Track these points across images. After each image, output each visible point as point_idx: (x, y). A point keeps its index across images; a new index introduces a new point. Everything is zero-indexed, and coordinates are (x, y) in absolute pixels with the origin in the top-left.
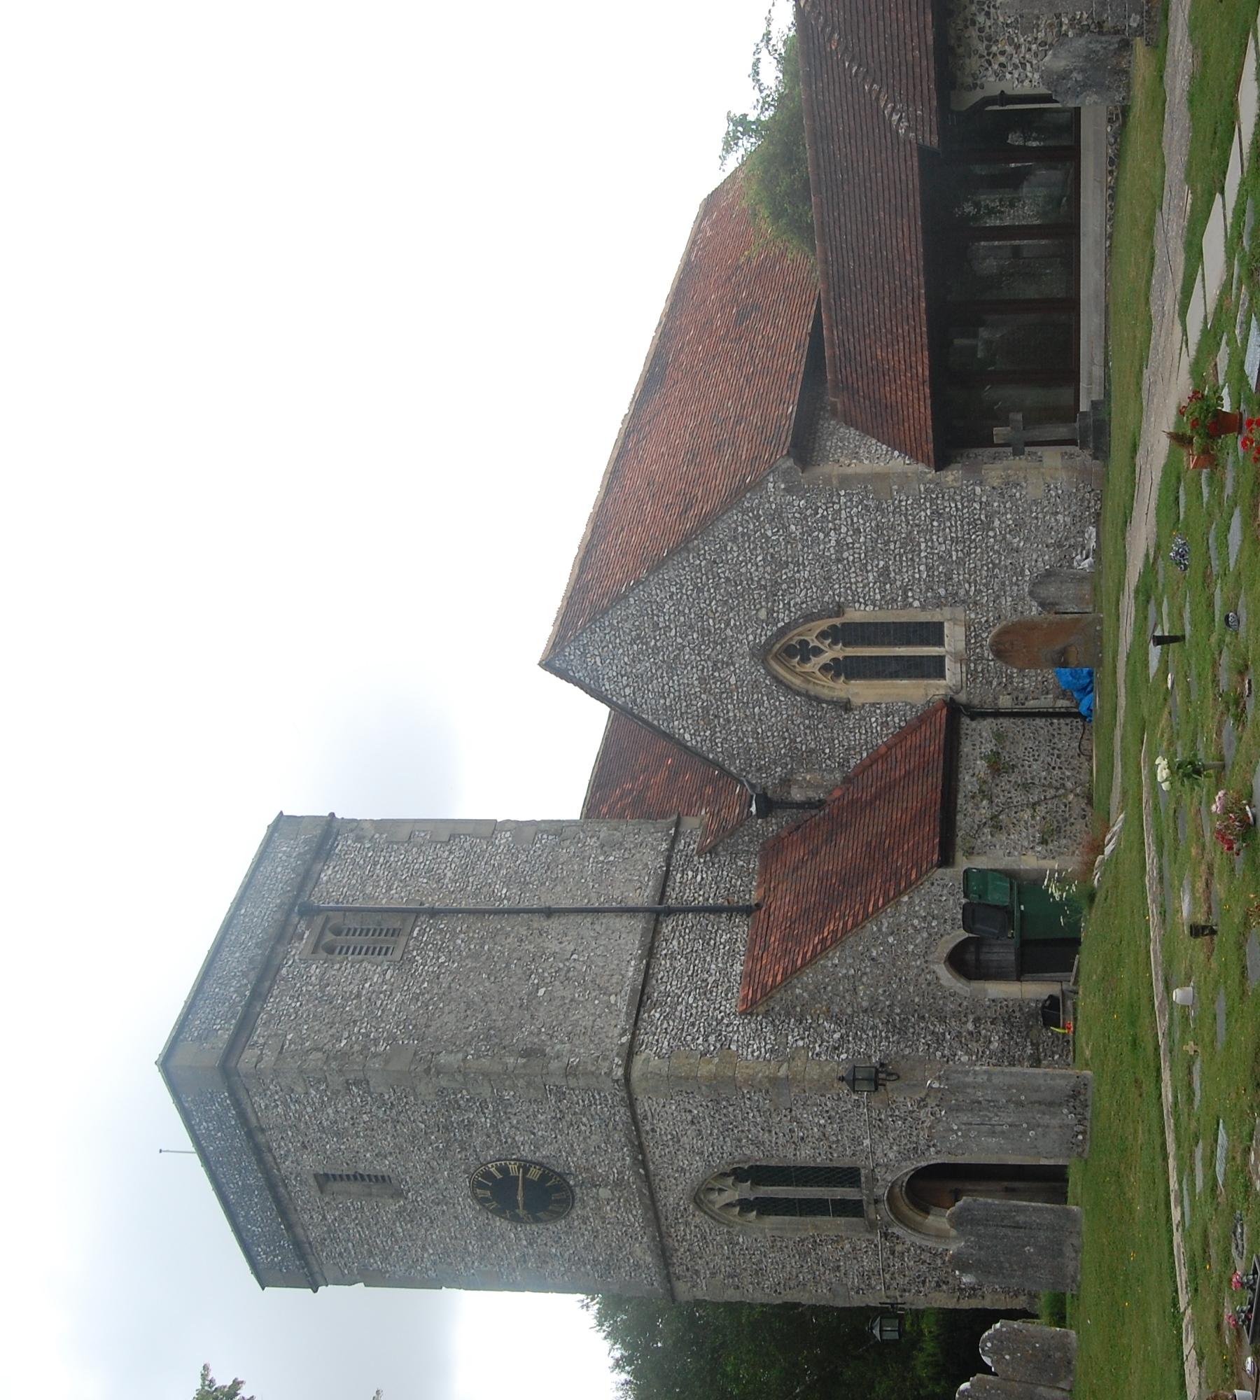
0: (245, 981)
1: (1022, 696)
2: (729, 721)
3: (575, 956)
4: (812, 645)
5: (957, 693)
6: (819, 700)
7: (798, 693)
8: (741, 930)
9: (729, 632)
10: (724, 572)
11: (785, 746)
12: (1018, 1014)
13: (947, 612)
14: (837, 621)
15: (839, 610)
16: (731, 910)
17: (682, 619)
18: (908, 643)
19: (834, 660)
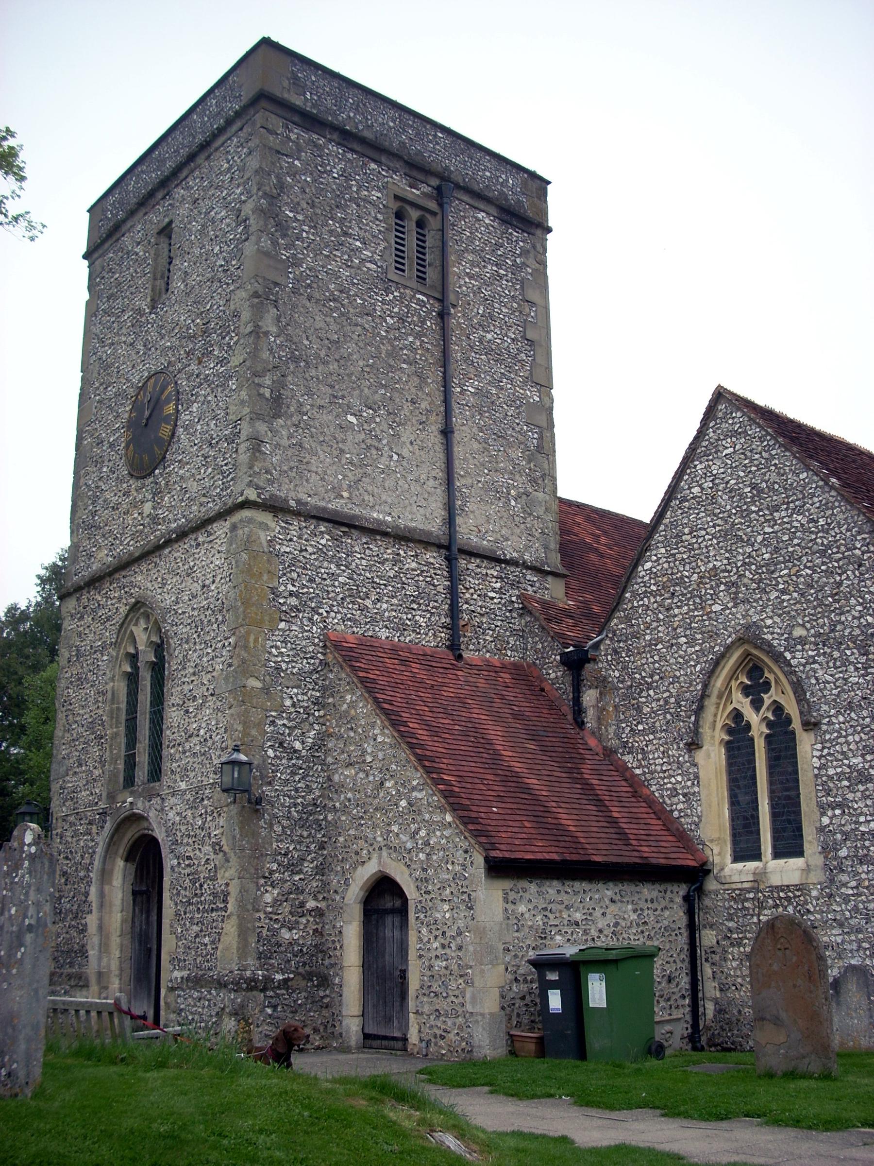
0: (361, 128)
1: (717, 958)
2: (668, 610)
3: (395, 457)
4: (765, 696)
5: (716, 878)
6: (700, 710)
7: (706, 686)
8: (431, 639)
9: (773, 595)
10: (848, 578)
11: (643, 678)
12: (327, 962)
13: (819, 860)
14: (796, 724)
15: (811, 725)
16: (454, 628)
17: (786, 538)
18: (775, 816)
19: (748, 726)
